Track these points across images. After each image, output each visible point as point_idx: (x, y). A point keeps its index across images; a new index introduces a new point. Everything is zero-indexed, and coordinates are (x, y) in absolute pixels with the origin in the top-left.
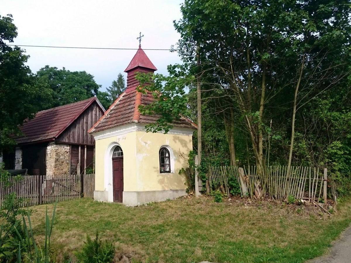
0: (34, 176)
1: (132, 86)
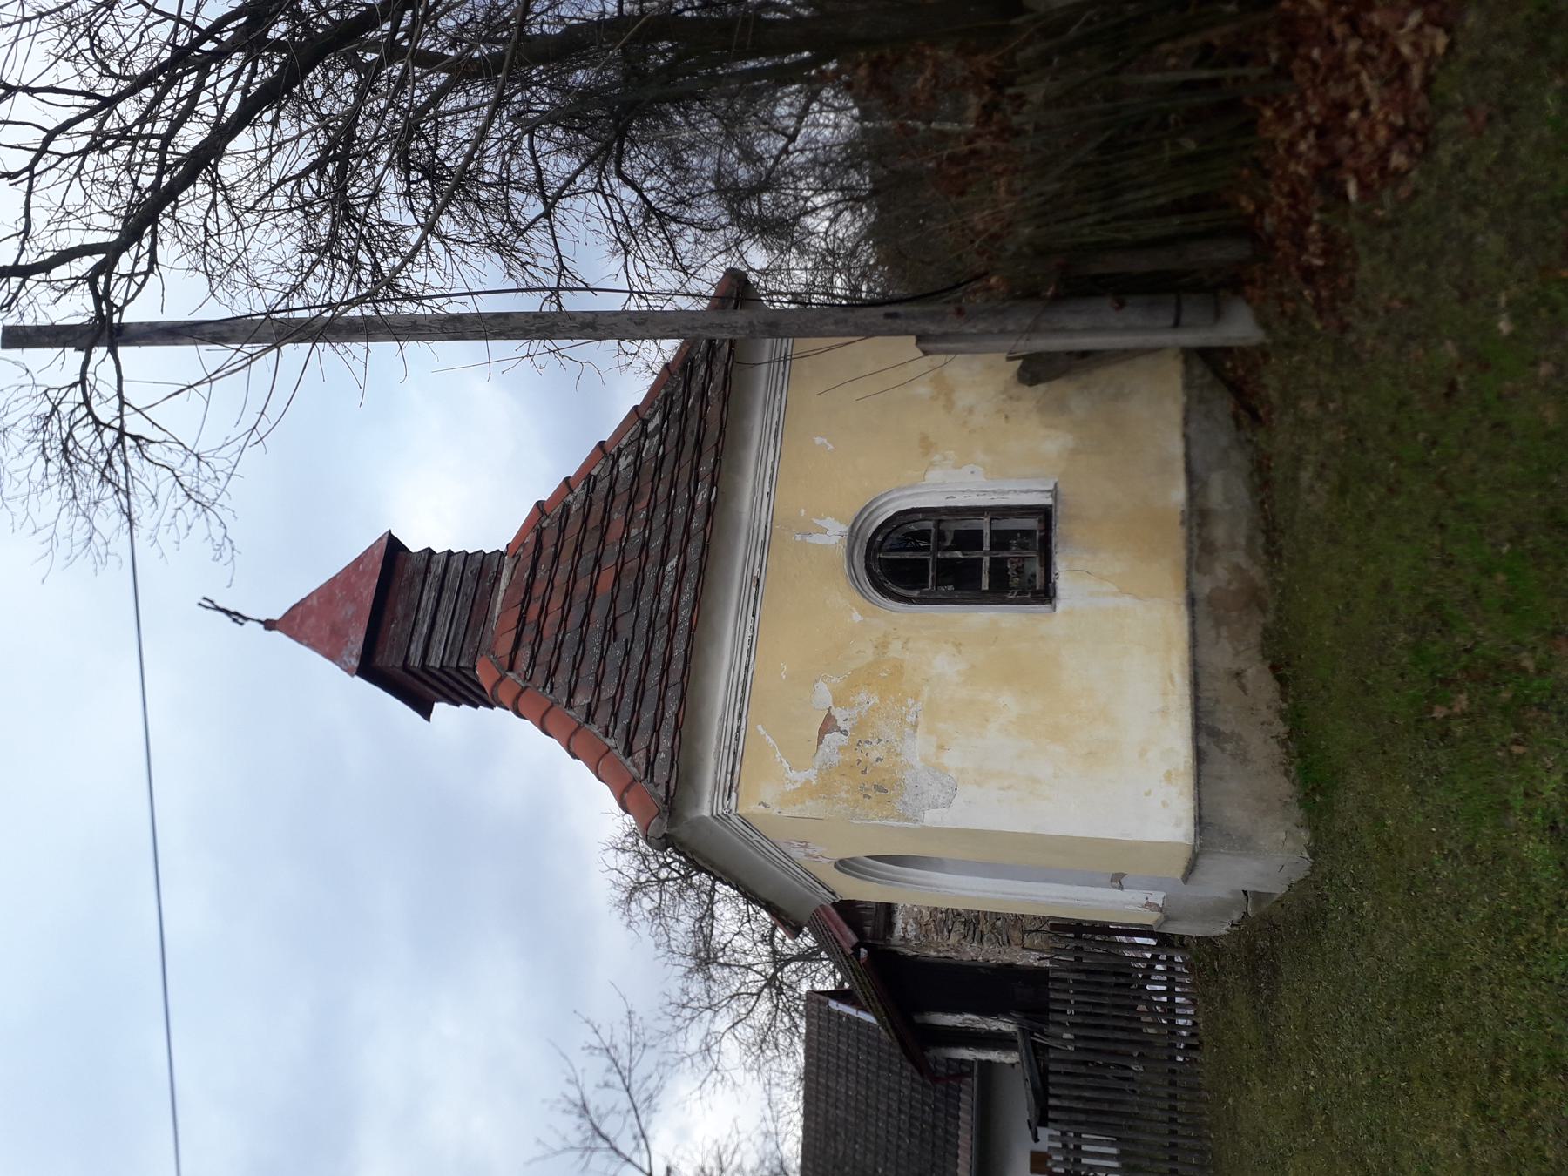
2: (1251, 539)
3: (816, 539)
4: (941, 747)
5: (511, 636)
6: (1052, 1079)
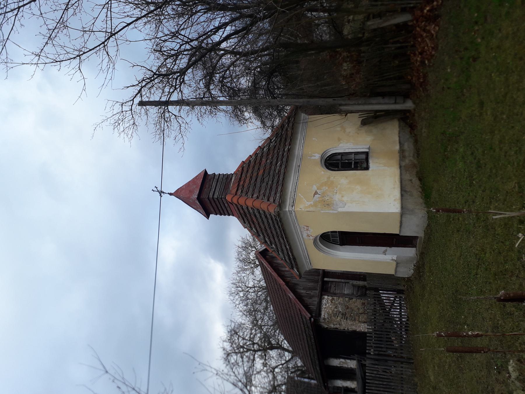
0: (367, 345)
1: (228, 209)
2: (413, 155)
3: (313, 158)
4: (343, 197)
5: (236, 189)
6: (367, 384)
